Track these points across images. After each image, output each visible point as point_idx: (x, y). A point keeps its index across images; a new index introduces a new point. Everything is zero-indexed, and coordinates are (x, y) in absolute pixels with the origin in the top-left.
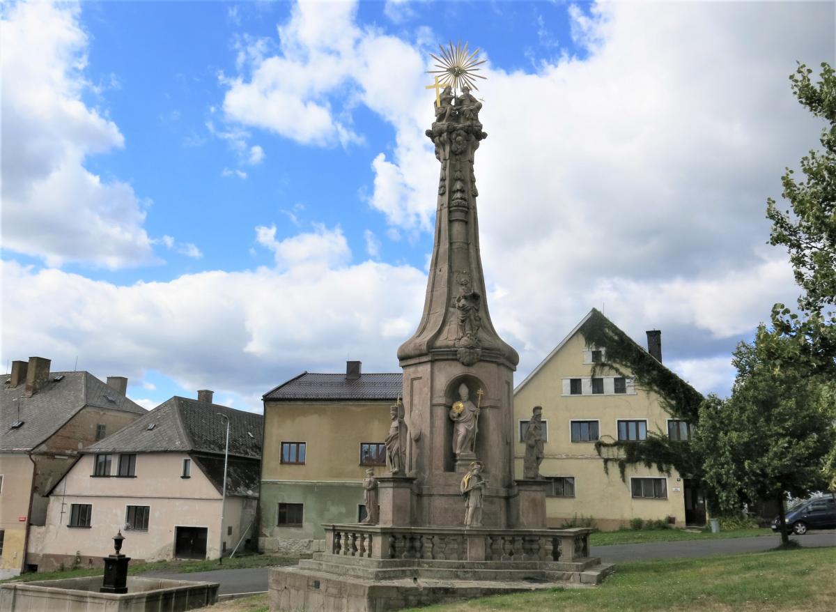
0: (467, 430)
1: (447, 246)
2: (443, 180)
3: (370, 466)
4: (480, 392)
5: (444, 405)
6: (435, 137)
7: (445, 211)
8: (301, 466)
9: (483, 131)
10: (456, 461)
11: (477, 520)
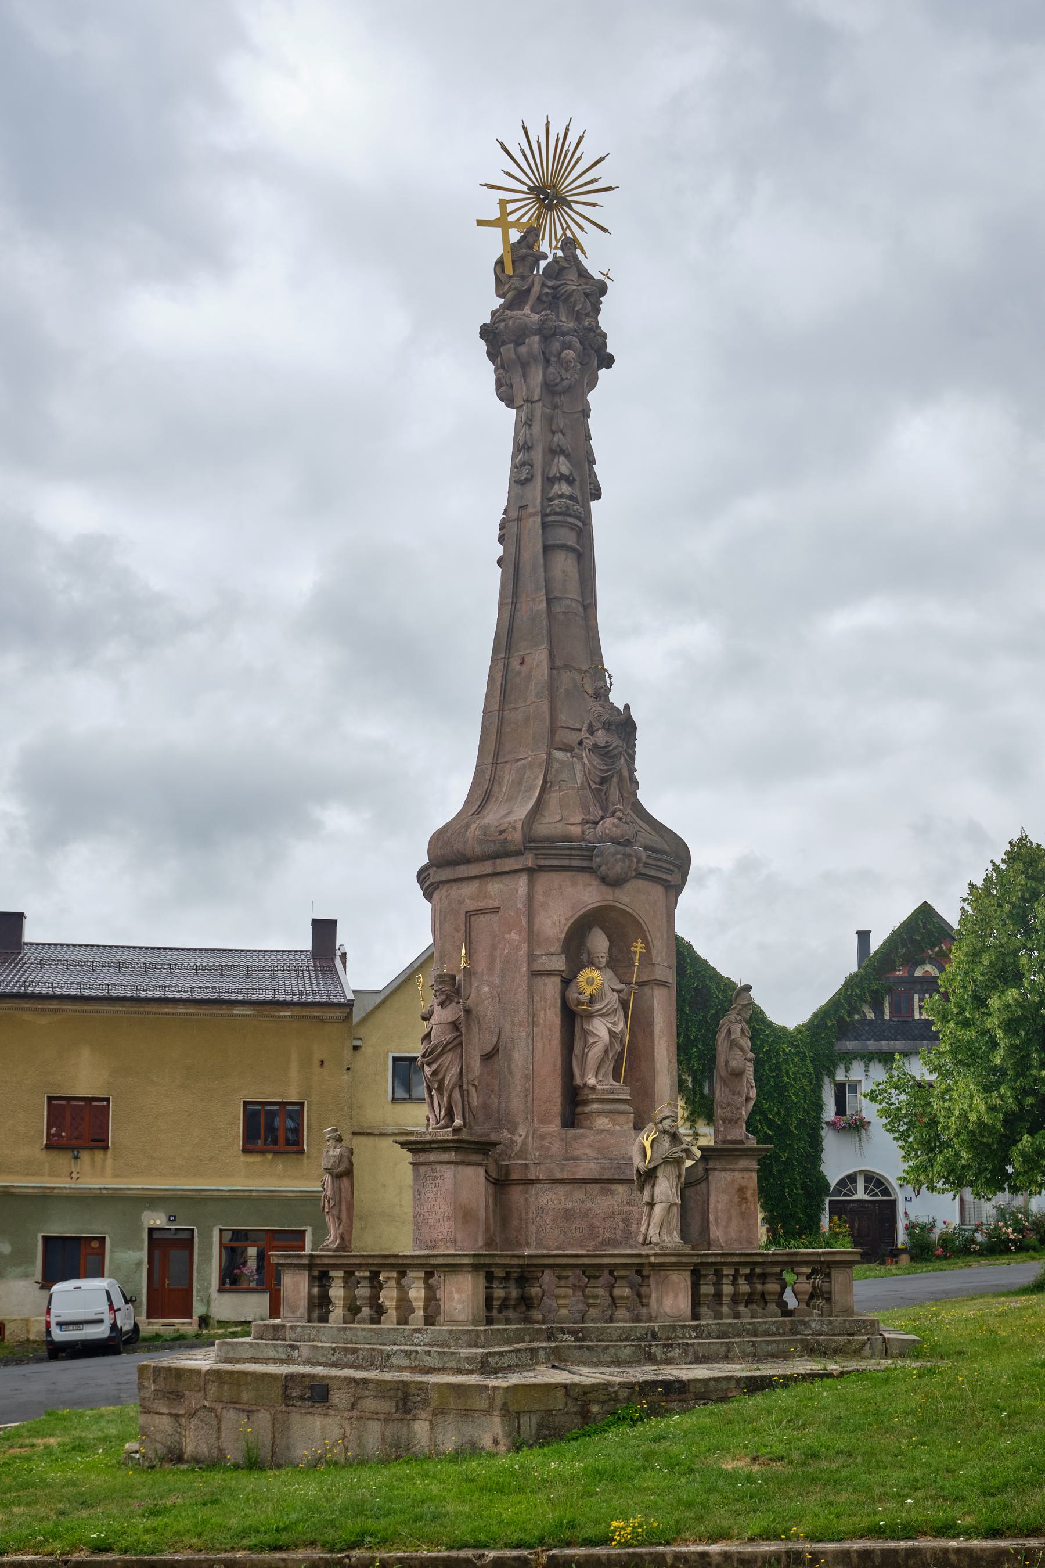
0: (611, 1033)
3: (72, 1148)
6: (504, 343)
10: (586, 1102)
11: (670, 1233)
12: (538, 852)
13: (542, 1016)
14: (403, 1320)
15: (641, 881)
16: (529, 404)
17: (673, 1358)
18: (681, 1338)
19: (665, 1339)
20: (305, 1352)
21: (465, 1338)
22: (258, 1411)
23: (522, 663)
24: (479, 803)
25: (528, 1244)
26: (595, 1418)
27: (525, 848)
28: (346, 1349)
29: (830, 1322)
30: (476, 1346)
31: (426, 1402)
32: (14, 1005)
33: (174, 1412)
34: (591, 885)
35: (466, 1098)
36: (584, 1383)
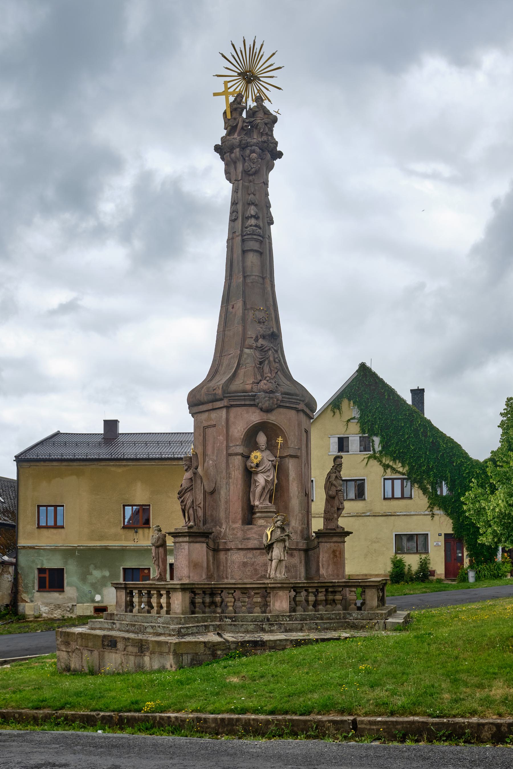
0: (266, 481)
1: (241, 280)
2: (234, 203)
3: (134, 528)
4: (280, 440)
5: (242, 455)
6: (225, 153)
7: (239, 239)
8: (60, 530)
9: (278, 149)
10: (255, 513)
11: (280, 573)
12: (230, 398)
13: (233, 474)
14: (158, 613)
15: (282, 409)
16: (237, 182)
17: (274, 630)
18: (281, 621)
19: (274, 621)
20: (118, 625)
21: (176, 620)
22: (94, 650)
23: (233, 308)
24: (212, 376)
25: (227, 578)
26: (219, 657)
27: (224, 397)
28: (131, 625)
29: (362, 614)
30: (180, 624)
31: (148, 648)
32: (106, 464)
33: (67, 650)
34: (255, 412)
35: (195, 513)
36: (214, 641)
